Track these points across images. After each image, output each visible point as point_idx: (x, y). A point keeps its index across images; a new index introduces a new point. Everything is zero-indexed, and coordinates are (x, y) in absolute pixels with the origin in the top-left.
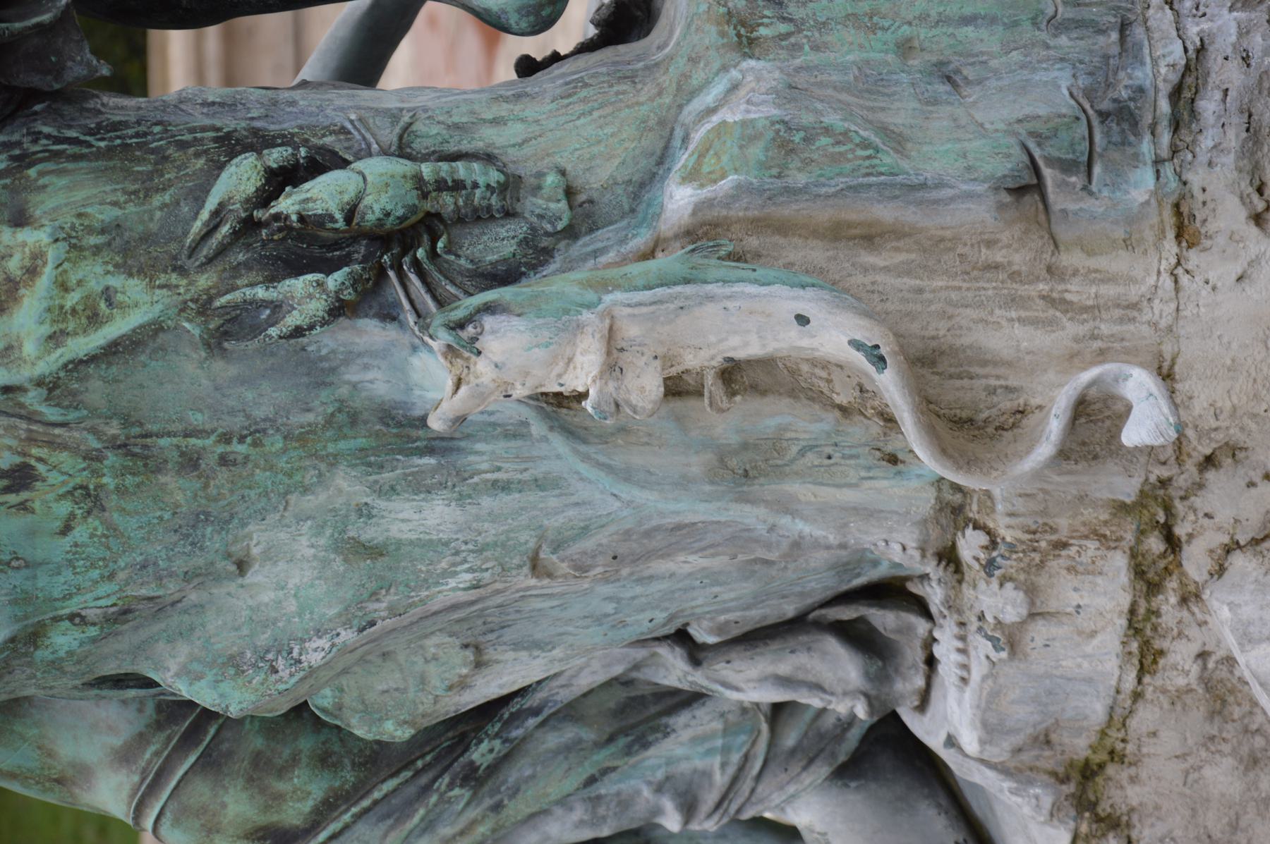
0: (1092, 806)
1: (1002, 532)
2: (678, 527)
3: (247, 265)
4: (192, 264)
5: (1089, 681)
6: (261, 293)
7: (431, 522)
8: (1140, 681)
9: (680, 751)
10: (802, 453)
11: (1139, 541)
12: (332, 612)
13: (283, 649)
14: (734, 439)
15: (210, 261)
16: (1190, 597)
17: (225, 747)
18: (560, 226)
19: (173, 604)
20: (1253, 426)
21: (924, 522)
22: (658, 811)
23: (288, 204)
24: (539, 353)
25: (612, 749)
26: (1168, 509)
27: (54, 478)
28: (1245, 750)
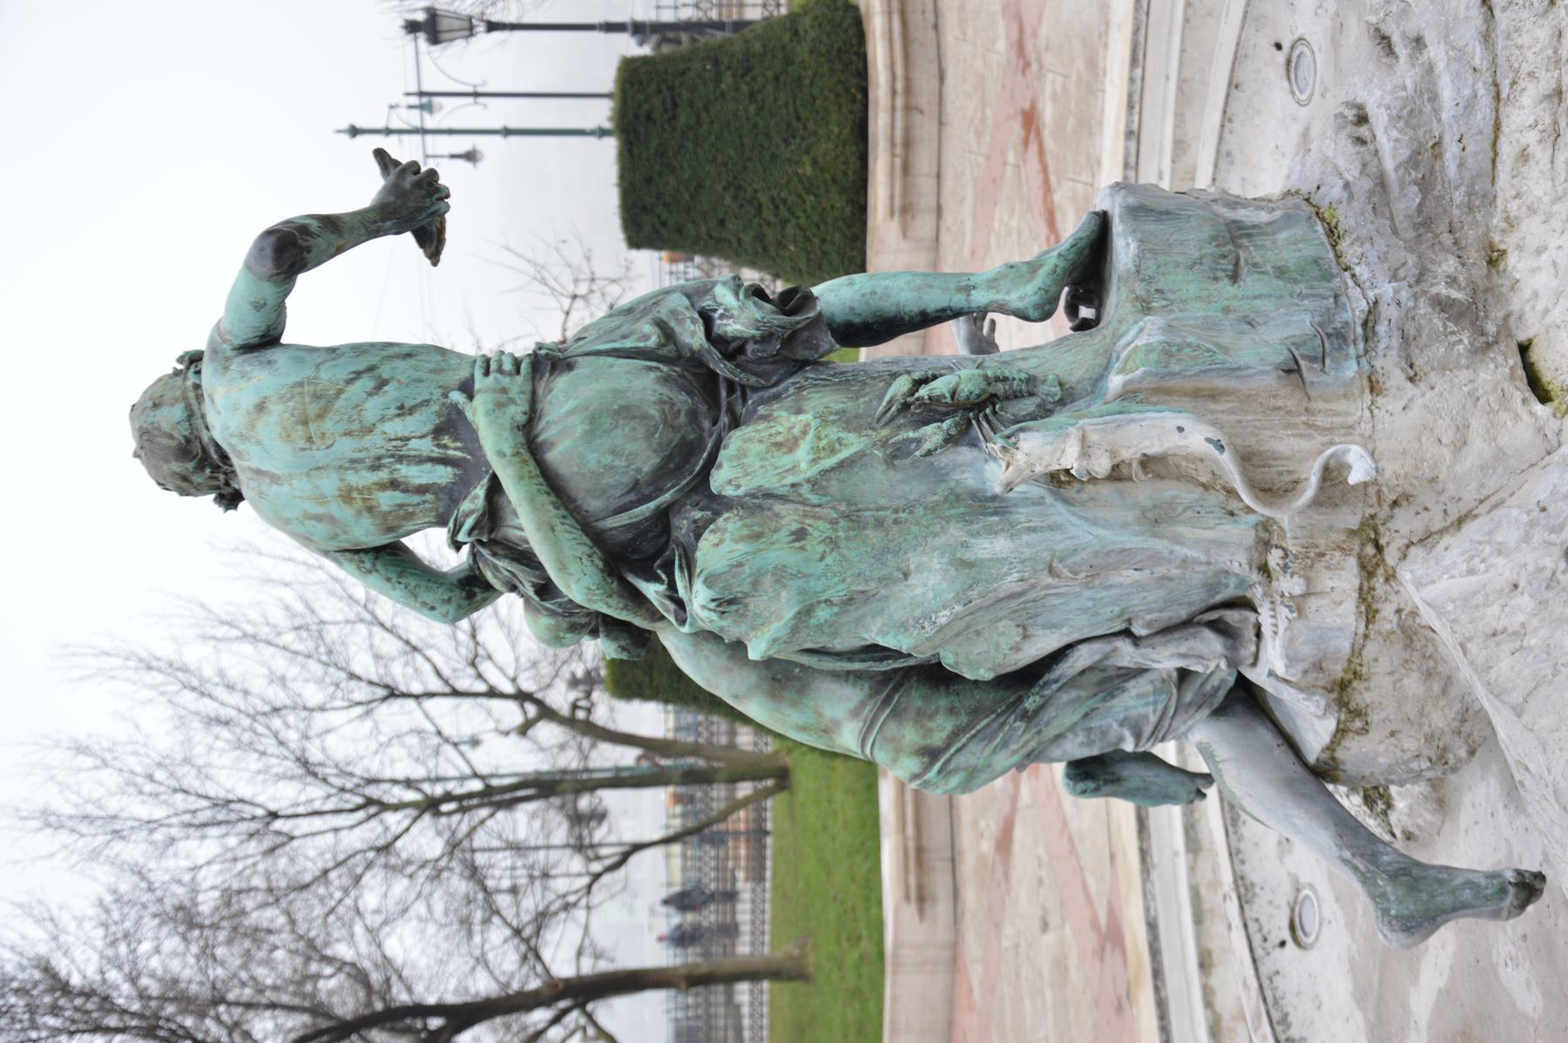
0: (1346, 705)
1: (1291, 548)
2: (1123, 550)
3: (905, 425)
4: (878, 426)
5: (1340, 629)
6: (911, 434)
7: (997, 549)
8: (1367, 627)
9: (1131, 703)
10: (1185, 510)
11: (1362, 550)
12: (950, 596)
13: (927, 617)
14: (1149, 503)
15: (887, 424)
16: (1390, 577)
17: (903, 705)
18: (1057, 398)
19: (874, 595)
20: (1416, 483)
21: (1250, 548)
22: (1121, 739)
23: (923, 392)
24: (1048, 448)
25: (1097, 698)
26: (1376, 531)
27: (816, 533)
28: (1424, 668)
